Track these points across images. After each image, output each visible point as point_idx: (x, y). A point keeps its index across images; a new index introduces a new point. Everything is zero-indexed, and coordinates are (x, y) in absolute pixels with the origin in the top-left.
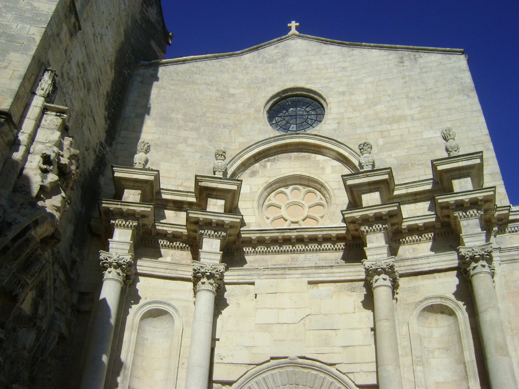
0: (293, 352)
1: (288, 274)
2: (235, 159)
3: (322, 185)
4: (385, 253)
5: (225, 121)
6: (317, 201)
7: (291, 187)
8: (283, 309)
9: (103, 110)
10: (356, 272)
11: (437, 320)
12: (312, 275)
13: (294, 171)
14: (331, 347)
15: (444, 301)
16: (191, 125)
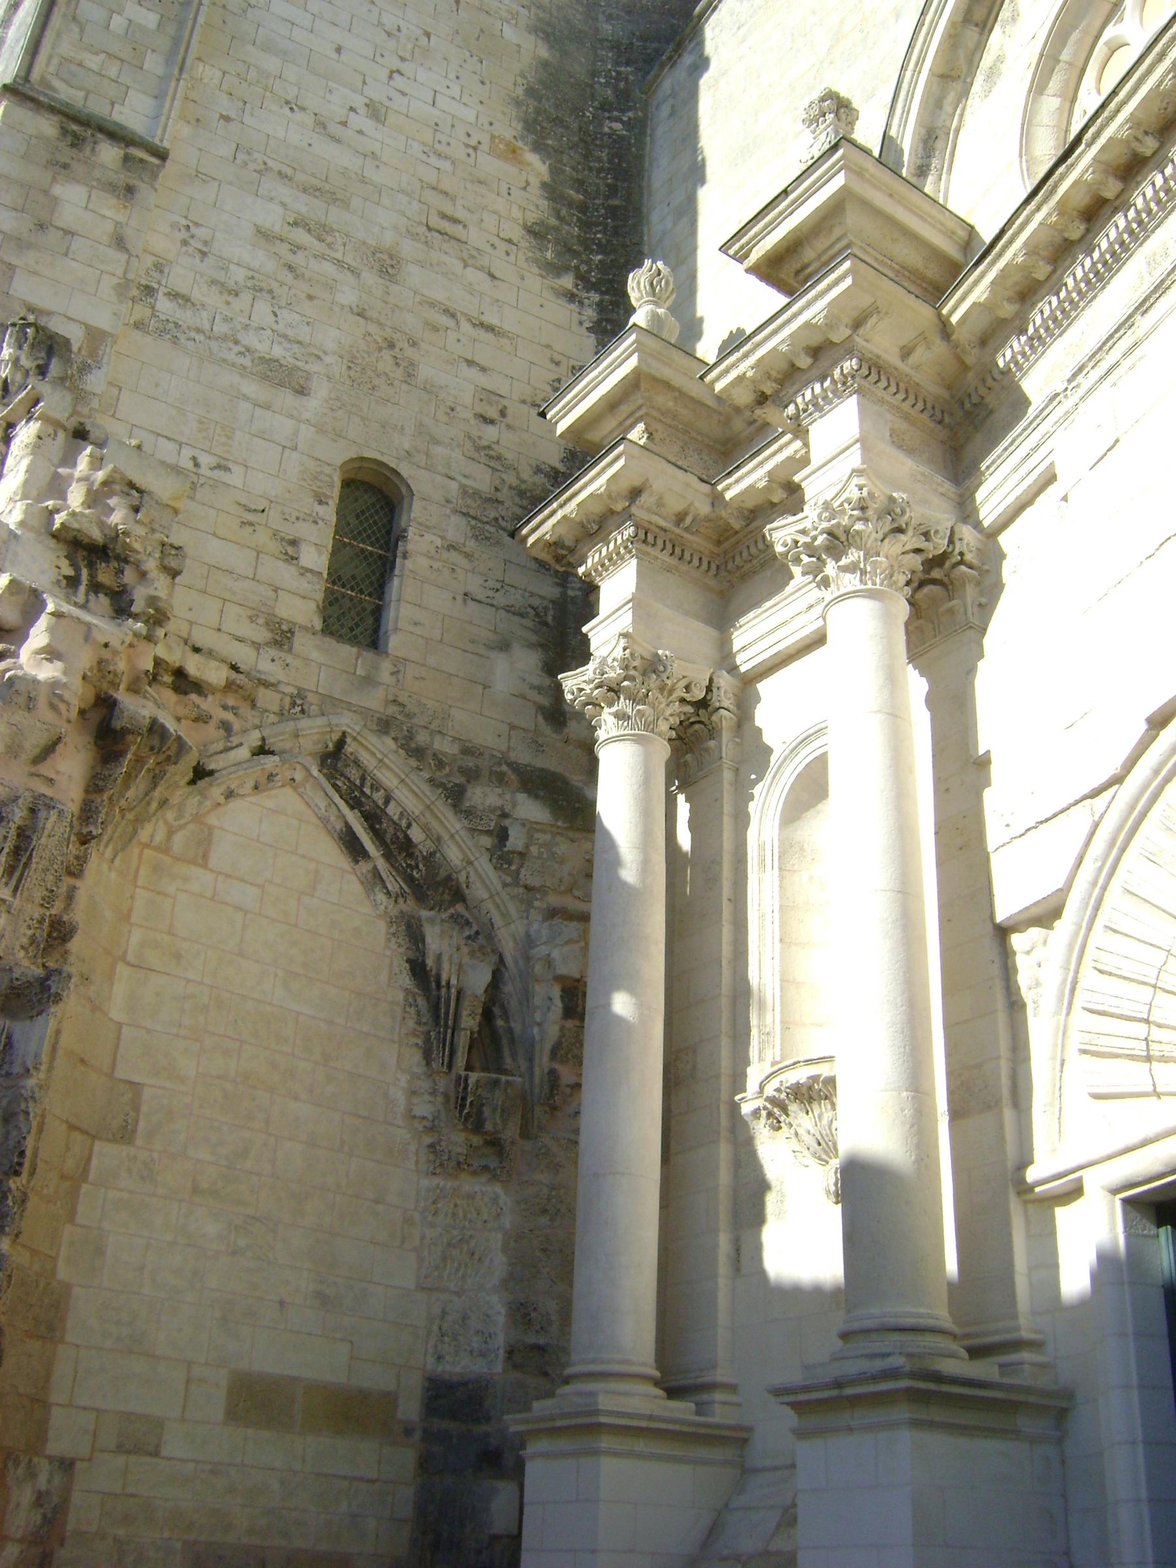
2: (905, 86)
9: (535, 282)
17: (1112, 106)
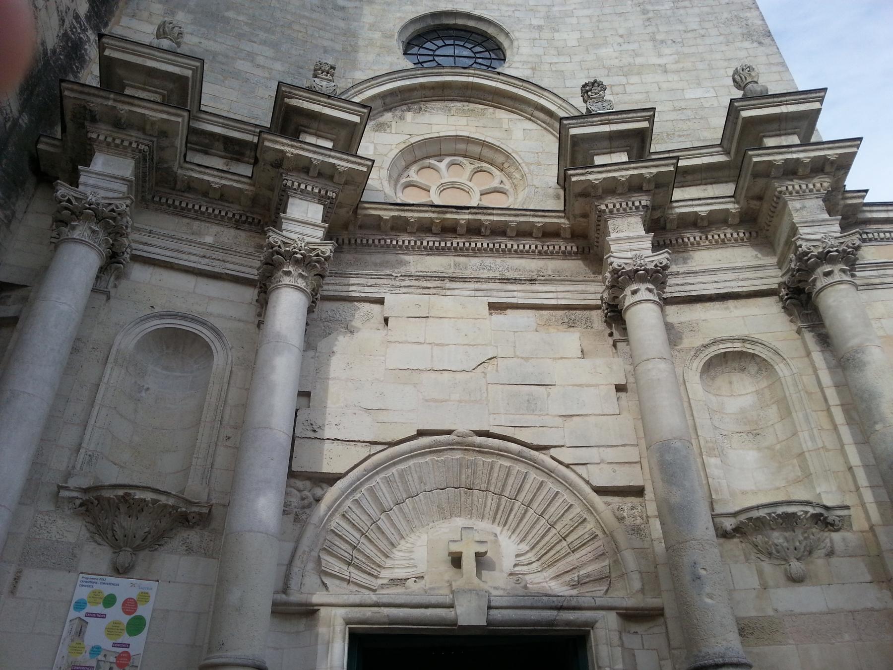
0: (463, 422)
1: (449, 289)
3: (508, 156)
4: (647, 249)
5: (326, 43)
6: (495, 184)
7: (447, 160)
8: (442, 345)
10: (577, 292)
11: (731, 383)
12: (495, 294)
13: (456, 130)
14: (540, 415)
15: (749, 346)
16: (263, 35)
17: (489, 211)
